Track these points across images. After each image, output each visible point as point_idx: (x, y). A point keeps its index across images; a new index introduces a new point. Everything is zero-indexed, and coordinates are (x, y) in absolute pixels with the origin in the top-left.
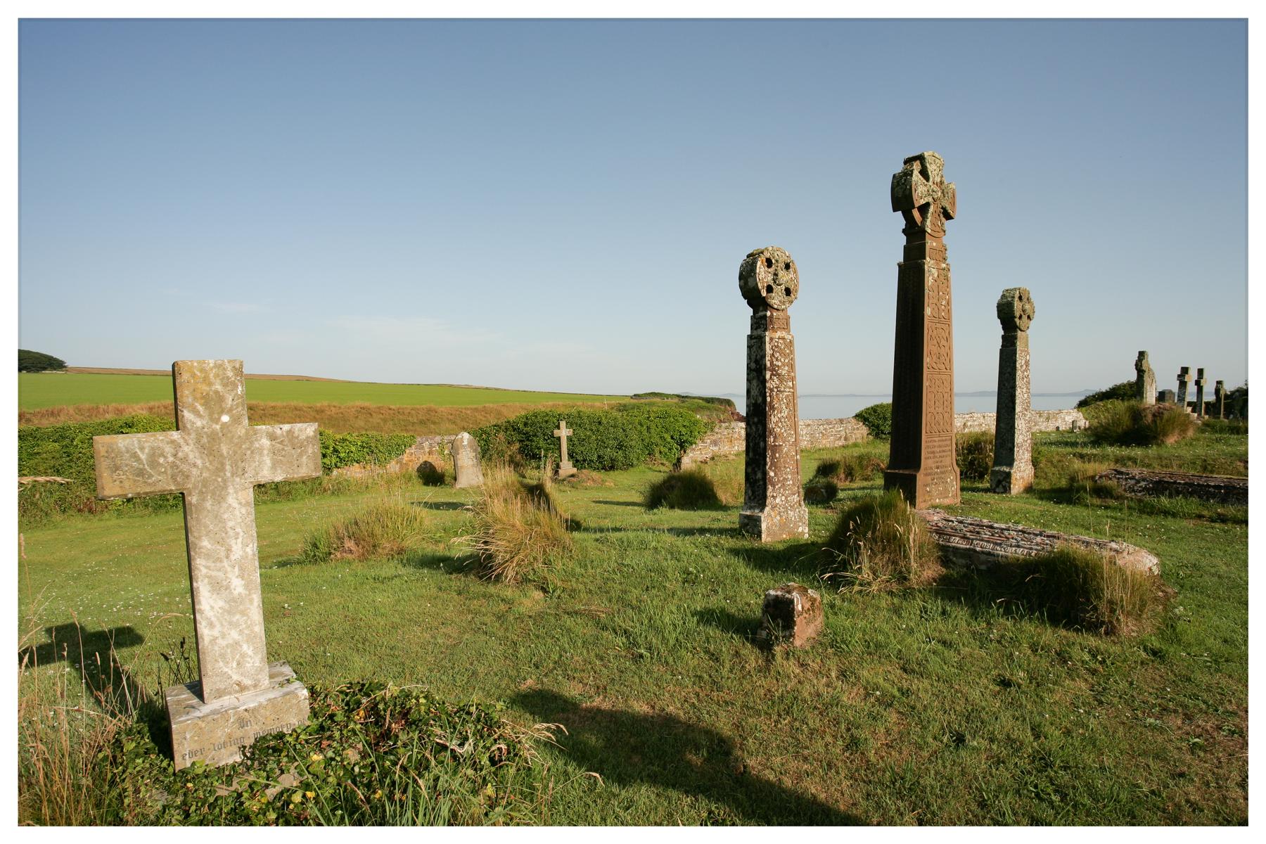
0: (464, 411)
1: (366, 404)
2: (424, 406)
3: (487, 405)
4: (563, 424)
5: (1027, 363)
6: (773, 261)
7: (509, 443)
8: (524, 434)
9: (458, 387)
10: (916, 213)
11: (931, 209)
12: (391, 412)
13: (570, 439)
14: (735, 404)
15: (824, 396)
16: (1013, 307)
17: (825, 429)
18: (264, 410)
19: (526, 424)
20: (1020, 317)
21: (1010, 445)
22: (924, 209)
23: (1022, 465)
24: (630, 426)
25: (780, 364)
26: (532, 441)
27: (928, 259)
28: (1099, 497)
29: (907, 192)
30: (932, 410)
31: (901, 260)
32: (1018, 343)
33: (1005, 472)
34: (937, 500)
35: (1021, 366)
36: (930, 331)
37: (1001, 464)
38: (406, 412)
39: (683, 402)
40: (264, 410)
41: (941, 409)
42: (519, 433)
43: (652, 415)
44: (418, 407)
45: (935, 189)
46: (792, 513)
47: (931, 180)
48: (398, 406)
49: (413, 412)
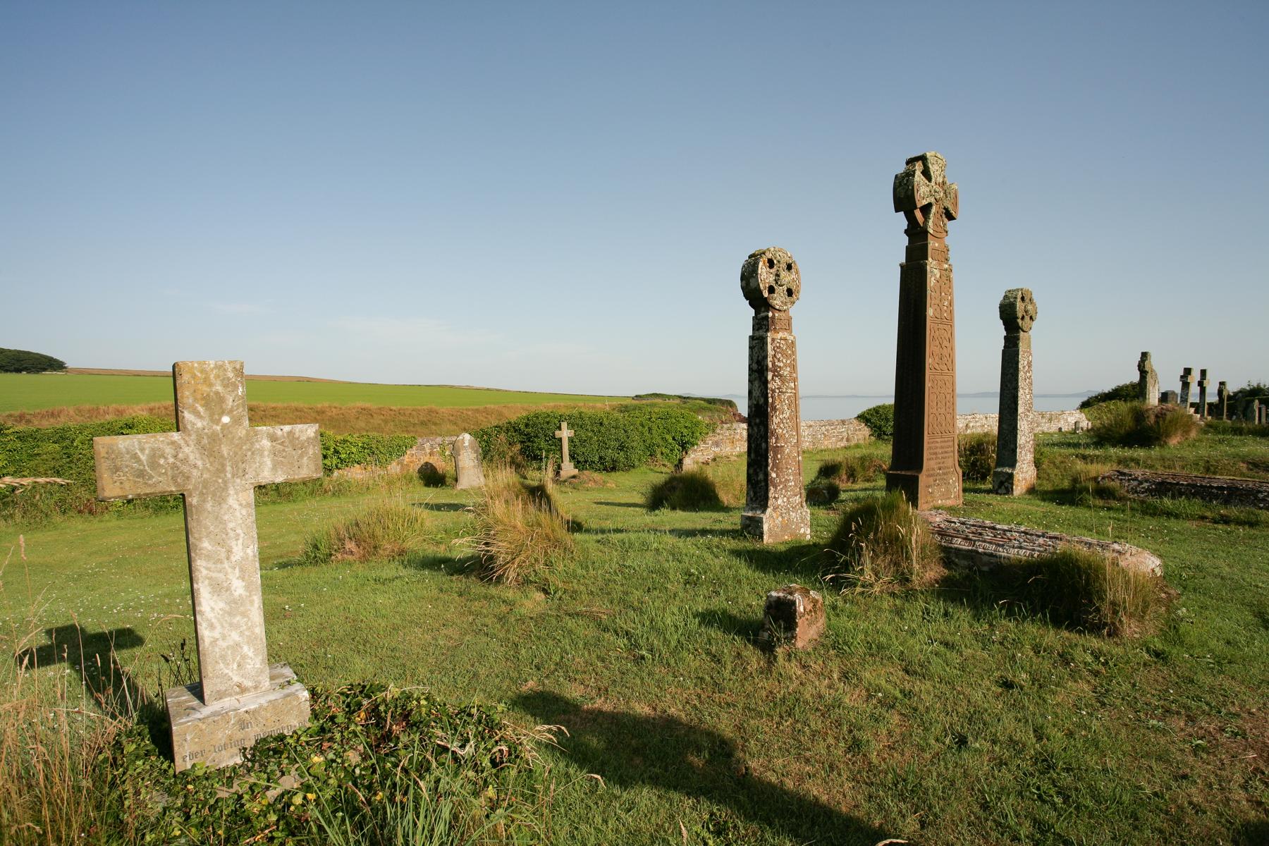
0: (465, 412)
1: (367, 405)
2: (425, 407)
3: (488, 406)
4: (564, 425)
5: (1030, 364)
6: (775, 262)
7: (510, 444)
8: (525, 435)
10: (918, 214)
11: (934, 210)
12: (392, 413)
15: (826, 397)
16: (1015, 308)
17: (827, 430)
18: (264, 411)
19: (527, 425)
20: (1023, 318)
21: (1012, 446)
22: (926, 209)
24: (632, 427)
25: (781, 365)
26: (533, 442)
27: (930, 259)
28: (1102, 498)
29: (910, 193)
30: (934, 411)
31: (903, 260)
32: (1021, 344)
33: (1007, 473)
34: (940, 502)
35: (1024, 367)
37: (1003, 466)
38: (407, 413)
39: (685, 403)
40: (264, 411)
42: (520, 434)
43: (654, 416)
44: (419, 408)
46: (794, 514)
47: (933, 180)
48: (399, 407)
49: (414, 413)
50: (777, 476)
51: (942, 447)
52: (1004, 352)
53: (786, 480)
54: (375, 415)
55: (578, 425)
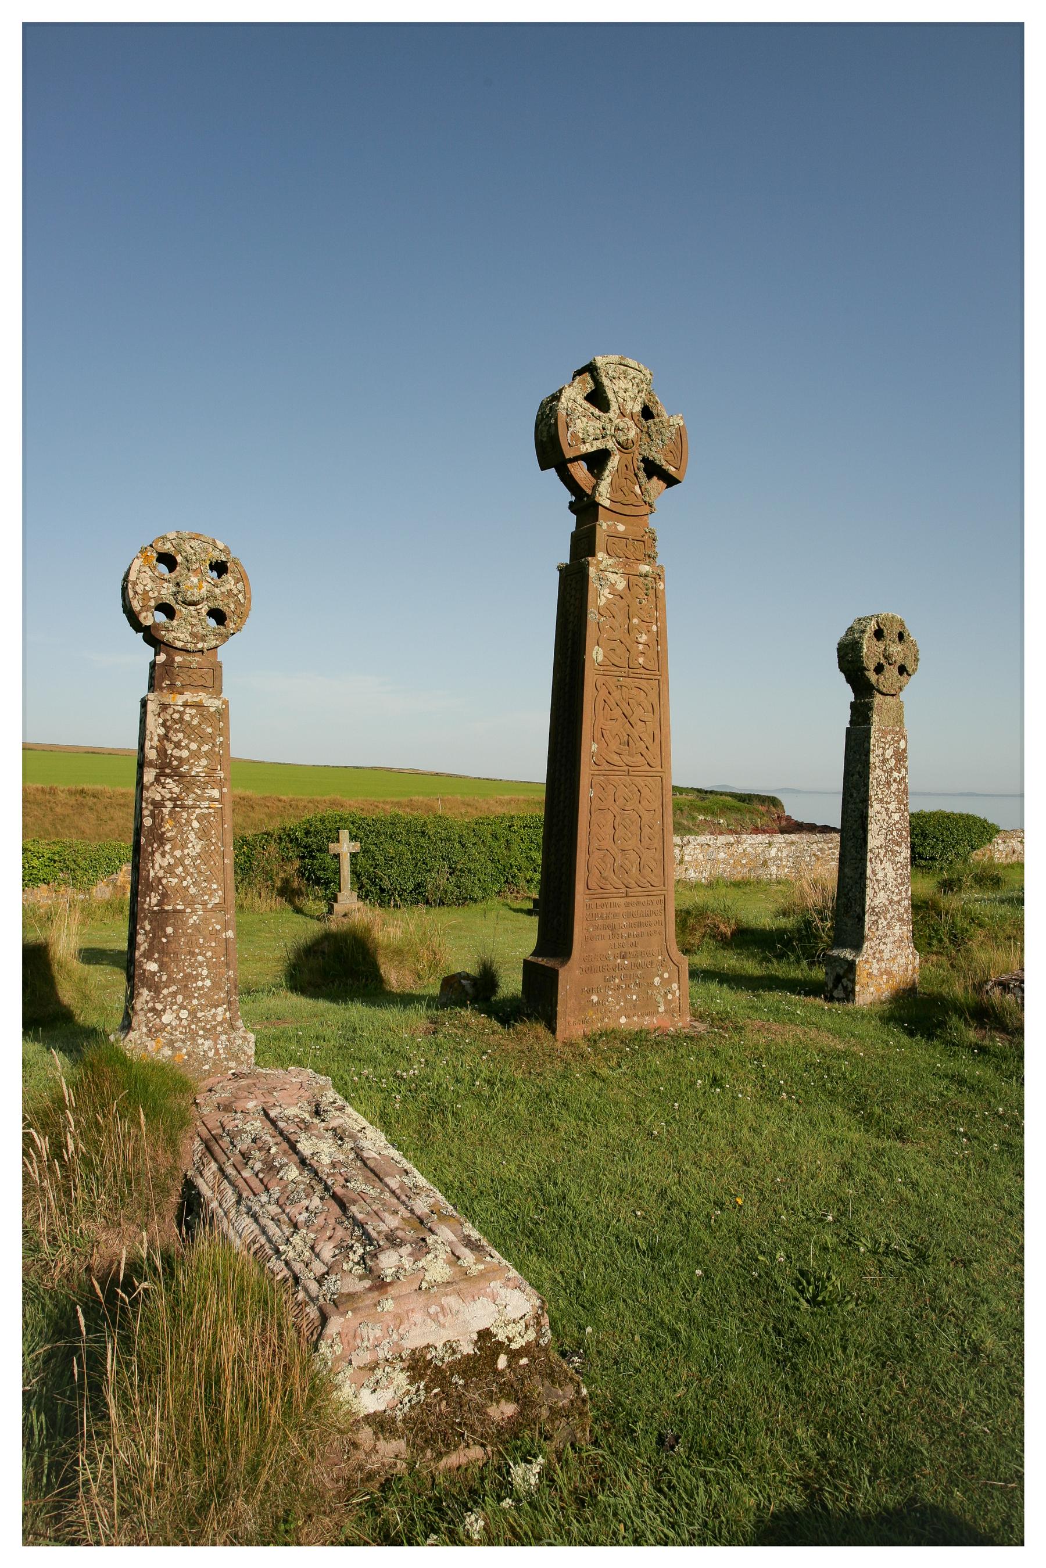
0: (381, 805)
1: (248, 793)
2: (327, 798)
3: (415, 798)
4: (344, 835)
5: (900, 756)
6: (179, 559)
7: (283, 860)
8: (305, 847)
9: (401, 772)
10: (580, 471)
11: (614, 463)
12: (280, 804)
13: (354, 856)
14: (784, 803)
15: (929, 794)
16: (860, 650)
17: (821, 850)
18: (110, 798)
19: (307, 833)
20: (879, 669)
21: (858, 909)
22: (597, 461)
23: (887, 950)
24: (475, 839)
25: (185, 754)
26: (314, 858)
27: (601, 555)
28: (982, 1026)
29: (553, 430)
30: (608, 843)
31: (566, 559)
32: (875, 718)
33: (845, 960)
34: (623, 1020)
35: (884, 761)
36: (603, 692)
37: (844, 946)
38: (301, 804)
39: (703, 799)
40: (110, 798)
41: (633, 842)
42: (299, 845)
43: (517, 822)
44: (319, 798)
45: (621, 425)
46: (208, 1043)
47: (614, 406)
48: (291, 796)
49: (311, 805)
50: (162, 967)
51: (629, 915)
52: (849, 731)
53: (188, 976)
54: (257, 807)
55: (386, 834)
